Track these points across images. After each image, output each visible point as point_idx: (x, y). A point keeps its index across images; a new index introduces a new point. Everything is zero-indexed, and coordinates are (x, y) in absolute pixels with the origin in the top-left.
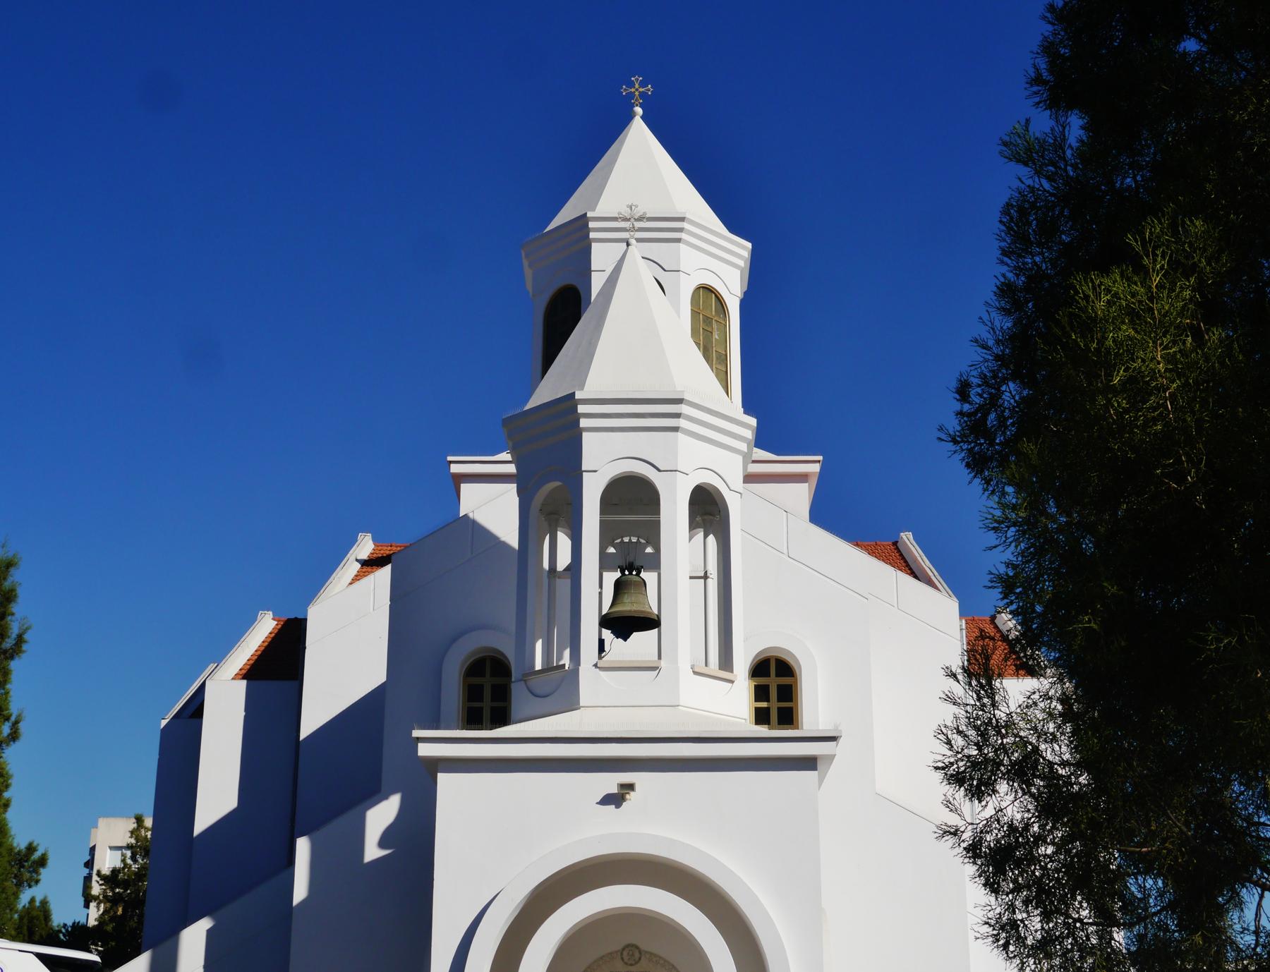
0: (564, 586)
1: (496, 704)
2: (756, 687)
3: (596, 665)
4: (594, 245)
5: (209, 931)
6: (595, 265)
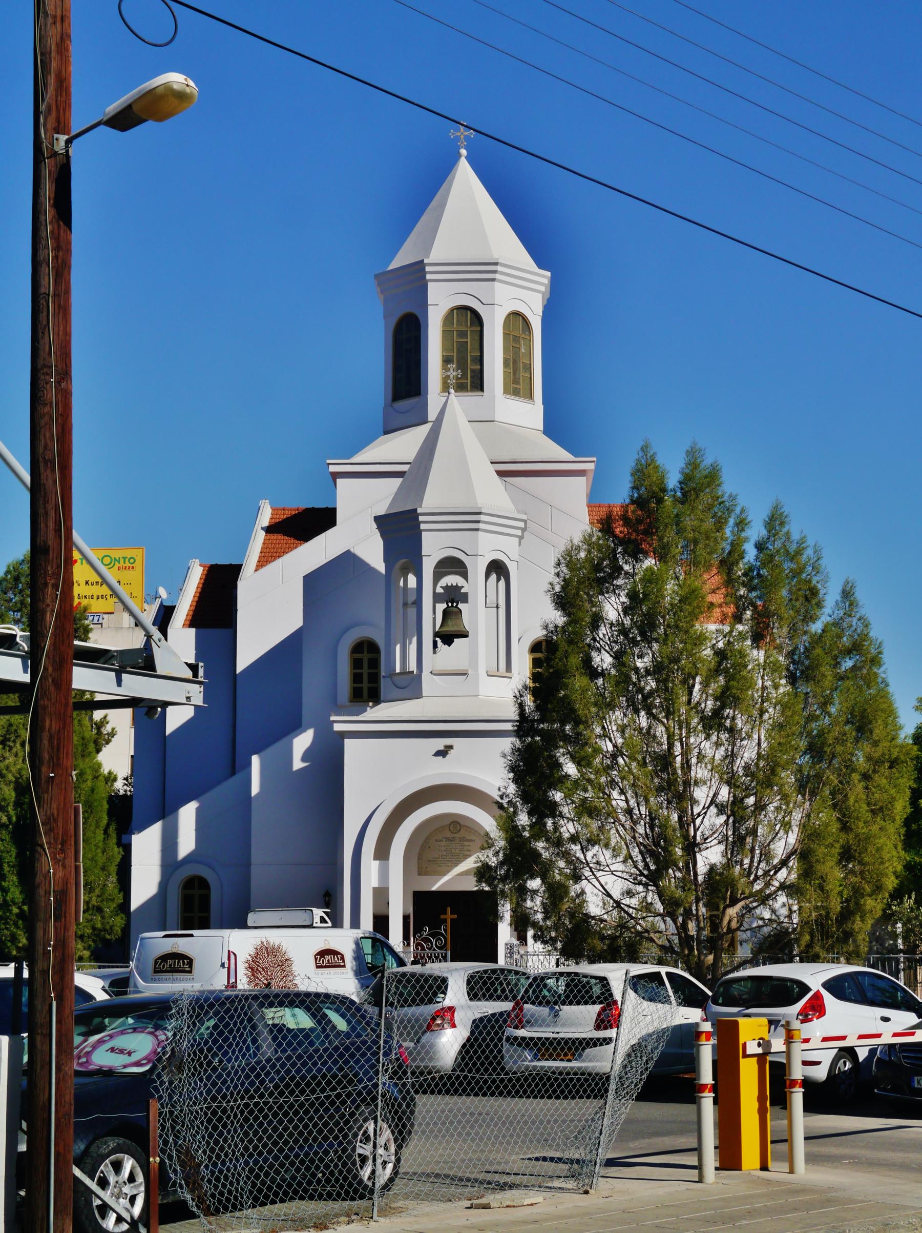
0: (412, 611)
1: (371, 685)
2: (534, 659)
3: (431, 673)
4: (430, 284)
5: (198, 810)
6: (424, 552)
